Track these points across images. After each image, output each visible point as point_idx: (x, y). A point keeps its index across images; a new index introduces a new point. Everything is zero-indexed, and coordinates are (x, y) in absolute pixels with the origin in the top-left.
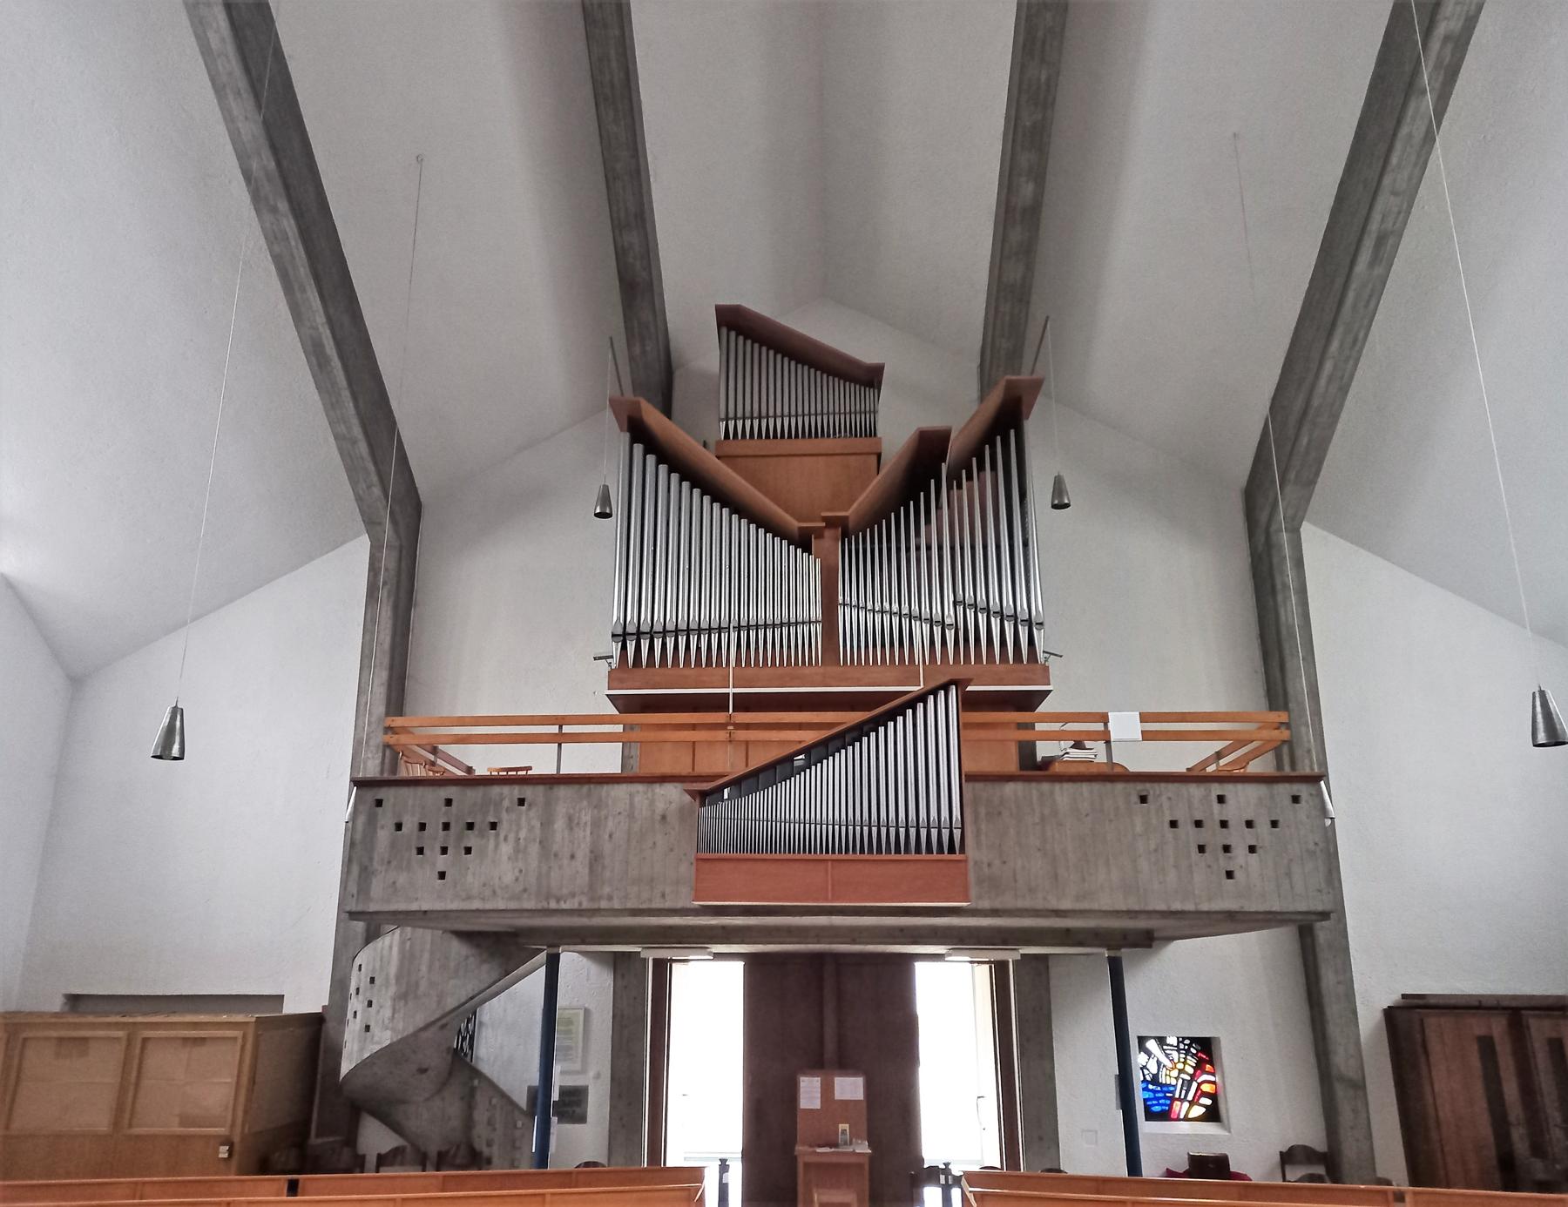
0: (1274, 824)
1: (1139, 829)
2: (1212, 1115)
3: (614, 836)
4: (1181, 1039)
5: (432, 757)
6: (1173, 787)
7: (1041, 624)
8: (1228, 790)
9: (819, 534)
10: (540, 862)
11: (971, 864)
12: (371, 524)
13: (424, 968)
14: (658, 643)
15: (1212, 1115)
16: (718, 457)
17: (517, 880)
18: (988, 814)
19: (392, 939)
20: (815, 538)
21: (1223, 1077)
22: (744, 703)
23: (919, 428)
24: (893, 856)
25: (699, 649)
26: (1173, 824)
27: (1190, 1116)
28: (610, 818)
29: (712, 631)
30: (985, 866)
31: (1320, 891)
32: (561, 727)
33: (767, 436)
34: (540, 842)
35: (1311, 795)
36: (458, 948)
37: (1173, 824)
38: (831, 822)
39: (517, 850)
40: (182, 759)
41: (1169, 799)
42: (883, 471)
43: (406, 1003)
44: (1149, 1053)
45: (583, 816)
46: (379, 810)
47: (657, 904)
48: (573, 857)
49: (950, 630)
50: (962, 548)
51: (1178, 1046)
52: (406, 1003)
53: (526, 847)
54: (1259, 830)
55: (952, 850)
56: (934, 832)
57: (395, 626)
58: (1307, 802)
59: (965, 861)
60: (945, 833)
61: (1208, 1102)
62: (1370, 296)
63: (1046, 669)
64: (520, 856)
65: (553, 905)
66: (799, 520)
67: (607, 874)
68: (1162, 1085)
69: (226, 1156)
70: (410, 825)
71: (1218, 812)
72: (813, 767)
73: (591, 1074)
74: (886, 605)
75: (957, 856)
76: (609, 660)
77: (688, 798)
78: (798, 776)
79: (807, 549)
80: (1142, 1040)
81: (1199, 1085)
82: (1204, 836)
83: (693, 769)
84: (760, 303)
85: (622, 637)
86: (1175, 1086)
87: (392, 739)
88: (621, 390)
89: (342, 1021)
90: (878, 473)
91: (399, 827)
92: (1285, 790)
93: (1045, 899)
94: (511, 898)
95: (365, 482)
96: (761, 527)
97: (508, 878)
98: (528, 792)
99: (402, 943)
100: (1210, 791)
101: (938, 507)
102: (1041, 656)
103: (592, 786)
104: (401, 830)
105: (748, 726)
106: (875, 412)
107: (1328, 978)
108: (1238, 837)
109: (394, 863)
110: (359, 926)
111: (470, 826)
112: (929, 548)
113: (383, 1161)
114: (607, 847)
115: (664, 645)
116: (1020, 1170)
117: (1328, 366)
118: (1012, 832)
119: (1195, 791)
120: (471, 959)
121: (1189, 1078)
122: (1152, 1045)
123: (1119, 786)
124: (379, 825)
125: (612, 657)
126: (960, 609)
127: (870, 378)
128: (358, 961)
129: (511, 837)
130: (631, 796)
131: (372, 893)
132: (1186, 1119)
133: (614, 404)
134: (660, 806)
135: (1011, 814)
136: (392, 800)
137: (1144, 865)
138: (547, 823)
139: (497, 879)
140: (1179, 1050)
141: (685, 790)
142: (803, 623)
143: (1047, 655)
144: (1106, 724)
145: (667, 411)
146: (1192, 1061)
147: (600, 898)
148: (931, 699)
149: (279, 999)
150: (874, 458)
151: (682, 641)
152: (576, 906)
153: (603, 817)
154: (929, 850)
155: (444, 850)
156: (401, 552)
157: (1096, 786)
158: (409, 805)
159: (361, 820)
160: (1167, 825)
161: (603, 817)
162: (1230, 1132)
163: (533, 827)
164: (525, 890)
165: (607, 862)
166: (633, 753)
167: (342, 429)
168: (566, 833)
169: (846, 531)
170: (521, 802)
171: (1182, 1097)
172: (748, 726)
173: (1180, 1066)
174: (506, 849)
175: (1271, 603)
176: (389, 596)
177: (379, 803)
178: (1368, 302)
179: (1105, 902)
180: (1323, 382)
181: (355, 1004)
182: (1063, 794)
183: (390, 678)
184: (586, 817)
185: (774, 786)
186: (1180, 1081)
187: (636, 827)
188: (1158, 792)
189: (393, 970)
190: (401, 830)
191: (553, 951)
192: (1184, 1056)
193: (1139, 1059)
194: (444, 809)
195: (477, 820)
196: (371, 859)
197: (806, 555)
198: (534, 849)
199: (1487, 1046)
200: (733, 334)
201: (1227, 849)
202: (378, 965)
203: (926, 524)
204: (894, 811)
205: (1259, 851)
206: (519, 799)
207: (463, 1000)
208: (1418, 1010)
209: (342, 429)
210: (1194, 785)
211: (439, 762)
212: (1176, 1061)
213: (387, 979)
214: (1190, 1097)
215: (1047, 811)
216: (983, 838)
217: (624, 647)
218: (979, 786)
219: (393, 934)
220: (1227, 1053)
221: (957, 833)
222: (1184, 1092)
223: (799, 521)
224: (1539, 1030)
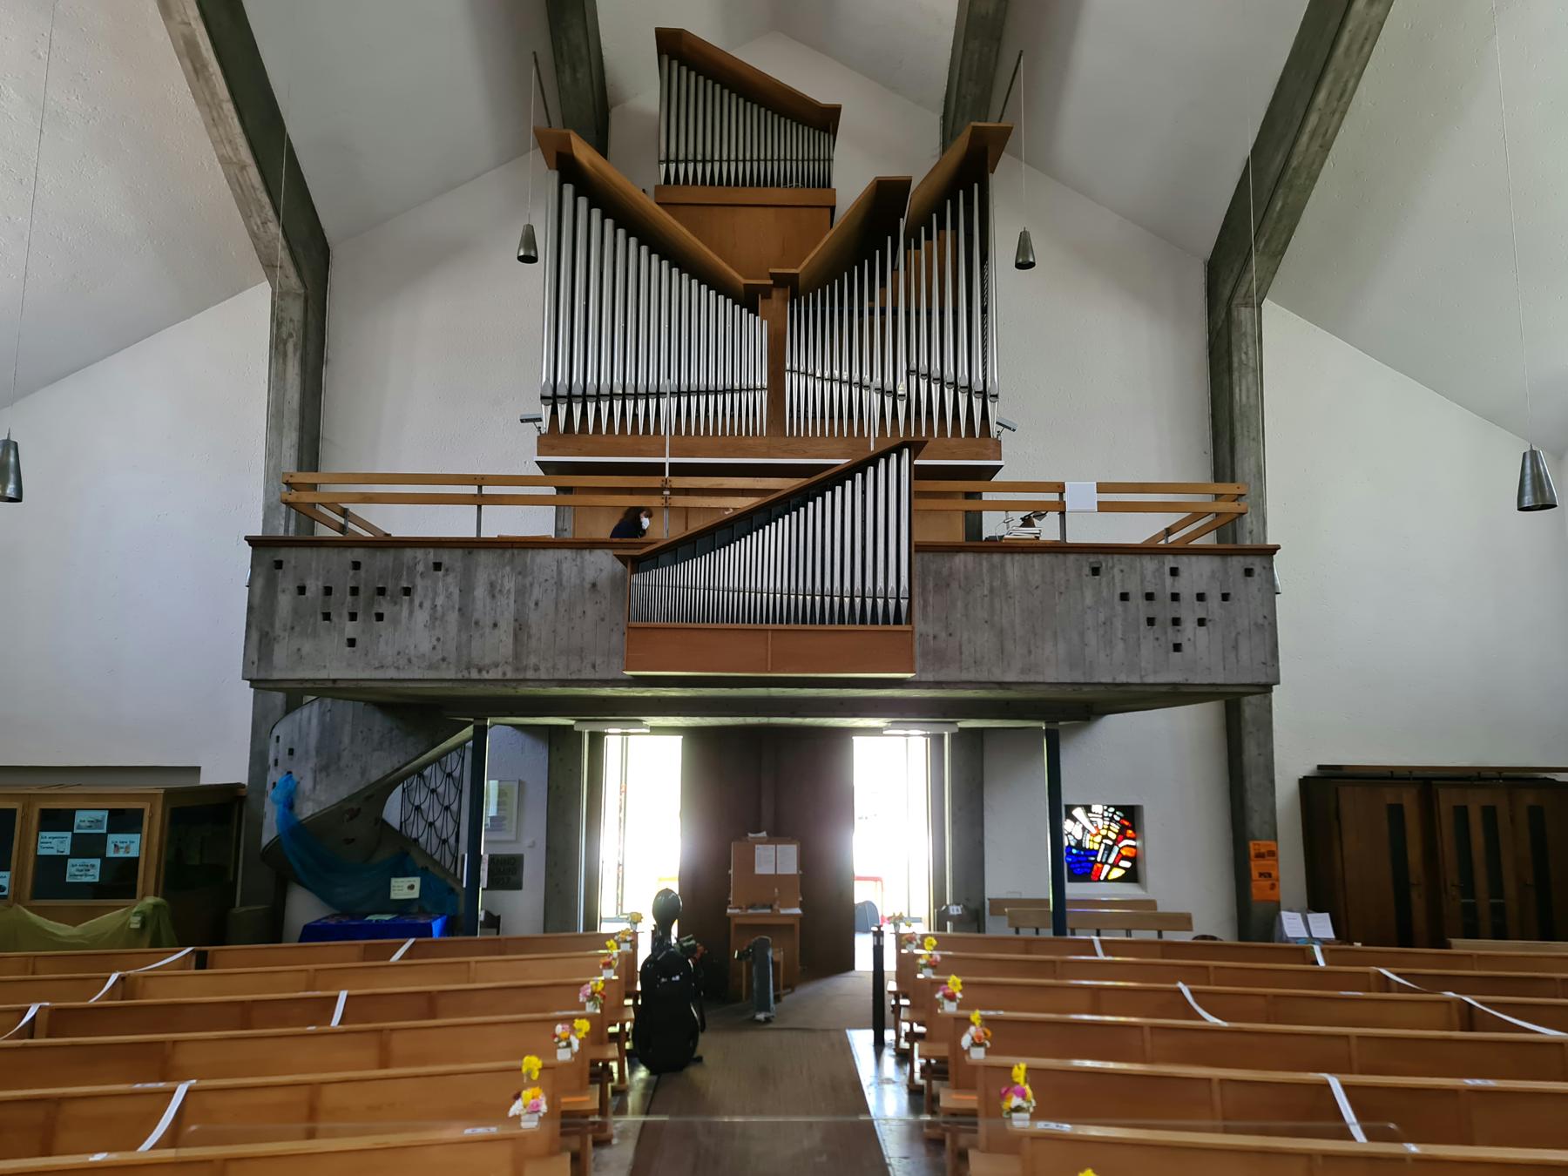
0: (1225, 597)
1: (1089, 601)
2: (1131, 876)
3: (540, 604)
4: (1106, 808)
5: (342, 521)
6: (1125, 559)
7: (996, 396)
8: (1183, 562)
9: (766, 292)
10: (459, 631)
11: (917, 636)
12: (269, 266)
13: (346, 740)
14: (591, 408)
15: (1131, 876)
16: (658, 204)
17: (434, 648)
18: (936, 585)
19: (311, 712)
20: (762, 299)
21: (1144, 843)
22: (677, 470)
23: (876, 178)
24: (836, 627)
25: (635, 415)
26: (1124, 597)
27: (1110, 877)
28: (536, 585)
29: (650, 396)
30: (931, 638)
31: (1264, 663)
32: (480, 488)
33: (712, 183)
34: (460, 610)
35: (1264, 568)
36: (379, 722)
37: (1124, 597)
38: (772, 591)
39: (433, 618)
40: (20, 501)
41: (1122, 571)
42: (836, 225)
43: (328, 775)
44: (1075, 820)
45: (506, 583)
46: (280, 572)
47: (588, 674)
48: (495, 625)
50: (918, 313)
51: (1102, 814)
52: (328, 775)
53: (443, 615)
54: (1209, 605)
55: (898, 621)
56: (880, 602)
57: (303, 382)
58: (1259, 575)
59: (912, 632)
60: (892, 603)
61: (1127, 864)
62: (1366, 39)
63: (999, 444)
64: (437, 623)
65: (474, 675)
66: (746, 278)
67: (533, 643)
69: (138, 926)
70: (314, 587)
71: (1170, 585)
72: (755, 534)
73: (527, 842)
74: (836, 373)
75: (904, 627)
76: (538, 424)
77: (620, 566)
78: (738, 542)
79: (754, 310)
80: (1070, 808)
81: (1120, 849)
82: (1154, 609)
84: (705, 27)
85: (552, 399)
86: (1097, 851)
87: (293, 496)
88: (549, 122)
89: (263, 793)
90: (831, 227)
91: (302, 590)
92: (1237, 563)
93: (989, 671)
94: (430, 667)
95: (259, 216)
96: (704, 284)
97: (425, 647)
98: (445, 556)
99: (322, 715)
100: (1164, 564)
101: (895, 269)
102: (994, 428)
103: (516, 551)
104: (304, 594)
105: (687, 492)
106: (830, 160)
107: (1251, 750)
108: (1189, 611)
109: (297, 629)
110: (279, 698)
111: (381, 591)
112: (883, 312)
113: (312, 933)
114: (533, 617)
115: (598, 410)
116: (946, 930)
117: (1313, 119)
118: (959, 604)
119: (1149, 564)
120: (395, 732)
123: (1072, 557)
124: (279, 589)
125: (540, 420)
126: (913, 379)
127: (825, 120)
128: (276, 732)
129: (427, 604)
130: (559, 563)
131: (275, 658)
132: (1106, 880)
133: (542, 139)
134: (590, 575)
135: (960, 586)
136: (293, 562)
137: (1092, 638)
138: (466, 590)
139: (413, 647)
141: (615, 555)
142: (748, 390)
143: (1000, 428)
144: (1061, 495)
145: (602, 148)
146: (1115, 828)
147: (525, 669)
148: (882, 462)
149: (196, 770)
150: (828, 211)
151: (617, 405)
152: (500, 676)
153: (528, 585)
154: (874, 621)
155: (353, 617)
156: (306, 301)
157: (1047, 558)
158: (315, 569)
159: (260, 583)
160: (1117, 597)
161: (528, 585)
162: (1146, 891)
163: (451, 594)
164: (444, 659)
165: (534, 631)
166: (566, 526)
167: (228, 151)
168: (488, 600)
169: (790, 286)
170: (437, 566)
171: (1104, 860)
172: (687, 492)
173: (1104, 832)
174: (422, 617)
175: (1226, 381)
176: (295, 350)
177: (279, 565)
178: (1362, 47)
179: (1051, 676)
180: (1304, 139)
181: (275, 776)
182: (1013, 567)
183: (301, 439)
184: (509, 584)
185: (713, 553)
187: (565, 596)
188: (1110, 564)
189: (313, 740)
190: (304, 594)
191: (480, 723)
192: (1108, 823)
193: (1068, 825)
194: (351, 572)
195: (390, 587)
196: (272, 625)
197: (751, 316)
198: (453, 617)
199: (1396, 812)
200: (675, 64)
201: (1176, 622)
202: (296, 738)
203: (880, 287)
204: (840, 583)
205: (1209, 624)
206: (435, 564)
207: (389, 772)
208: (1332, 780)
209: (228, 151)
210: (1148, 557)
211: (351, 526)
212: (1100, 827)
213: (307, 752)
214: (1111, 860)
215: (996, 583)
216: (930, 609)
217: (554, 412)
218: (927, 556)
219: (312, 705)
220: (1149, 820)
221: (904, 603)
222: (1105, 855)
223: (746, 278)
224: (1447, 800)
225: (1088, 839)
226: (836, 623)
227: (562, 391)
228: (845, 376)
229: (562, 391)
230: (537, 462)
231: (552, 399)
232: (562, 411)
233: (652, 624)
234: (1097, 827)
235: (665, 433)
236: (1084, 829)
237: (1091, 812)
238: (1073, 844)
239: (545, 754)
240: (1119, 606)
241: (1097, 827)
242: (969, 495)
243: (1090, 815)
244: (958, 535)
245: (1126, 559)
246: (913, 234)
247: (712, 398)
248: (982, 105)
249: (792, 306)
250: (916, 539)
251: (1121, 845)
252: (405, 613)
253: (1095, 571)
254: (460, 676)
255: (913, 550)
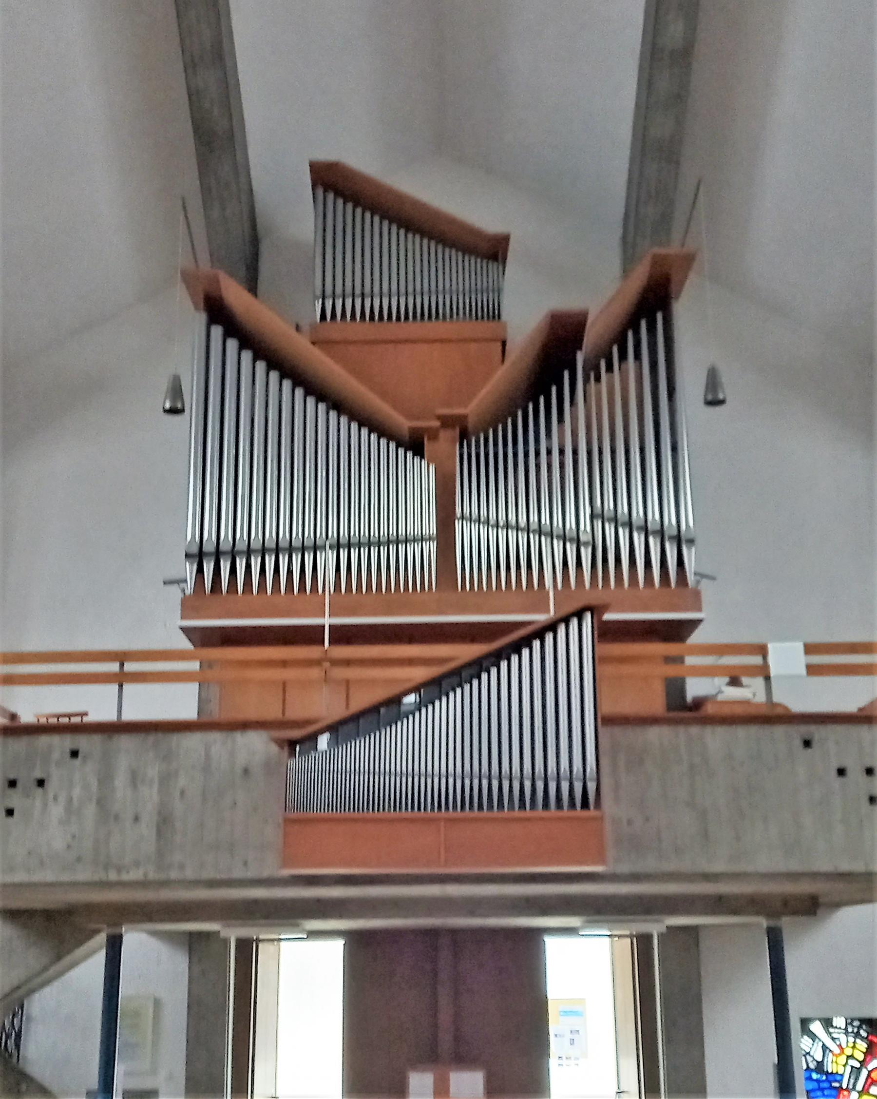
9: (434, 435)
17: (69, 847)
25: (290, 572)
26: (841, 772)
32: (122, 665)
44: (813, 1037)
47: (238, 873)
49: (586, 548)
51: (846, 1029)
55: (585, 804)
59: (601, 819)
65: (113, 876)
68: (827, 1073)
73: (163, 1074)
75: (592, 812)
76: (183, 585)
77: (274, 748)
79: (419, 452)
80: (805, 1023)
81: (870, 1072)
83: (283, 714)
85: (199, 557)
86: (842, 1075)
90: (503, 361)
97: (59, 844)
98: (83, 742)
102: (691, 578)
105: (348, 663)
114: (178, 807)
115: (248, 566)
121: (858, 1065)
122: (816, 1027)
126: (598, 524)
129: (62, 799)
133: (188, 279)
134: (241, 759)
138: (106, 779)
140: (847, 1033)
145: (252, 286)
146: (862, 1046)
160: (834, 773)
164: (79, 859)
165: (178, 825)
170: (74, 754)
171: (851, 1087)
172: (348, 663)
173: (848, 1051)
174: (57, 811)
179: (764, 863)
184: (153, 772)
186: (848, 1069)
191: (114, 931)
198: (90, 811)
214: (859, 1087)
217: (200, 570)
222: (852, 1081)
225: (830, 1061)
226: (517, 808)
227: (209, 547)
228: (523, 522)
229: (209, 547)
230: (183, 629)
231: (199, 557)
232: (208, 568)
233: (311, 814)
234: (840, 1046)
235: (324, 590)
236: (825, 1048)
237: (832, 1026)
238: (812, 1066)
239: (37, 996)
240: (837, 782)
241: (840, 1046)
242: (669, 660)
243: (831, 1030)
244: (657, 704)
245: (840, 730)
246: (592, 369)
247: (374, 551)
248: (664, 221)
249: (461, 446)
250: (607, 708)
251: (870, 1067)
252: (38, 803)
253: (807, 744)
254: (96, 878)
255: (599, 720)
